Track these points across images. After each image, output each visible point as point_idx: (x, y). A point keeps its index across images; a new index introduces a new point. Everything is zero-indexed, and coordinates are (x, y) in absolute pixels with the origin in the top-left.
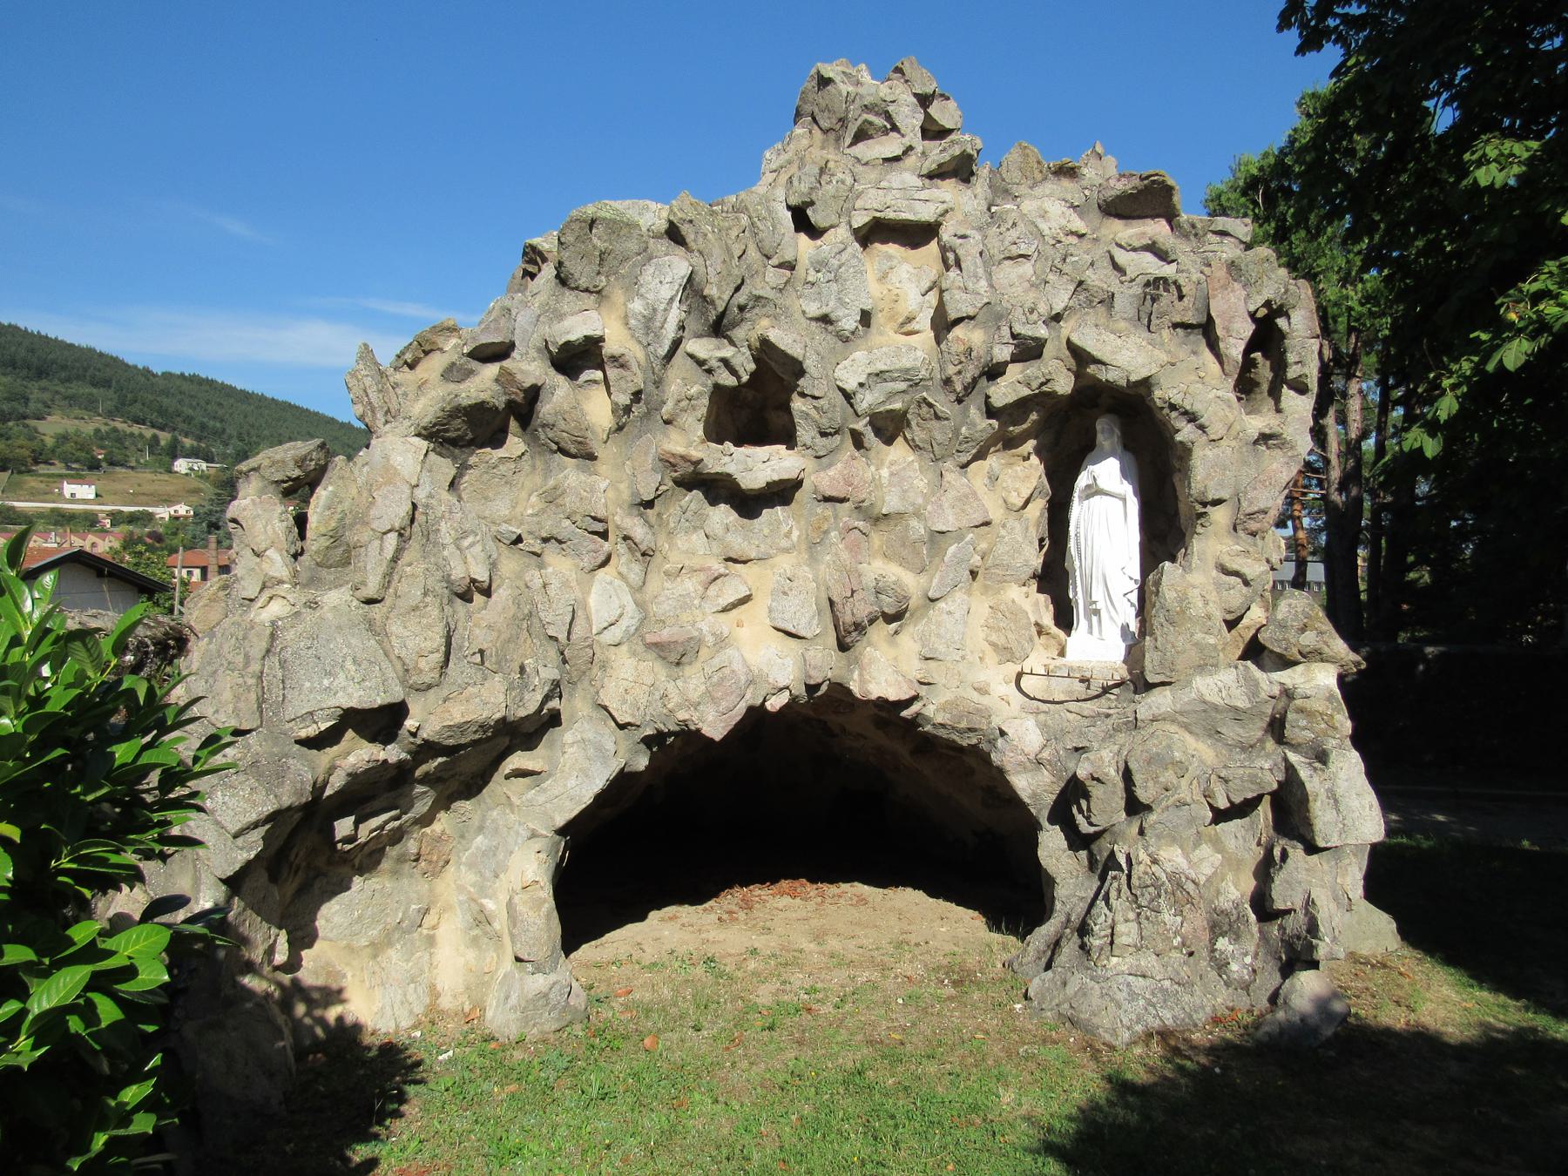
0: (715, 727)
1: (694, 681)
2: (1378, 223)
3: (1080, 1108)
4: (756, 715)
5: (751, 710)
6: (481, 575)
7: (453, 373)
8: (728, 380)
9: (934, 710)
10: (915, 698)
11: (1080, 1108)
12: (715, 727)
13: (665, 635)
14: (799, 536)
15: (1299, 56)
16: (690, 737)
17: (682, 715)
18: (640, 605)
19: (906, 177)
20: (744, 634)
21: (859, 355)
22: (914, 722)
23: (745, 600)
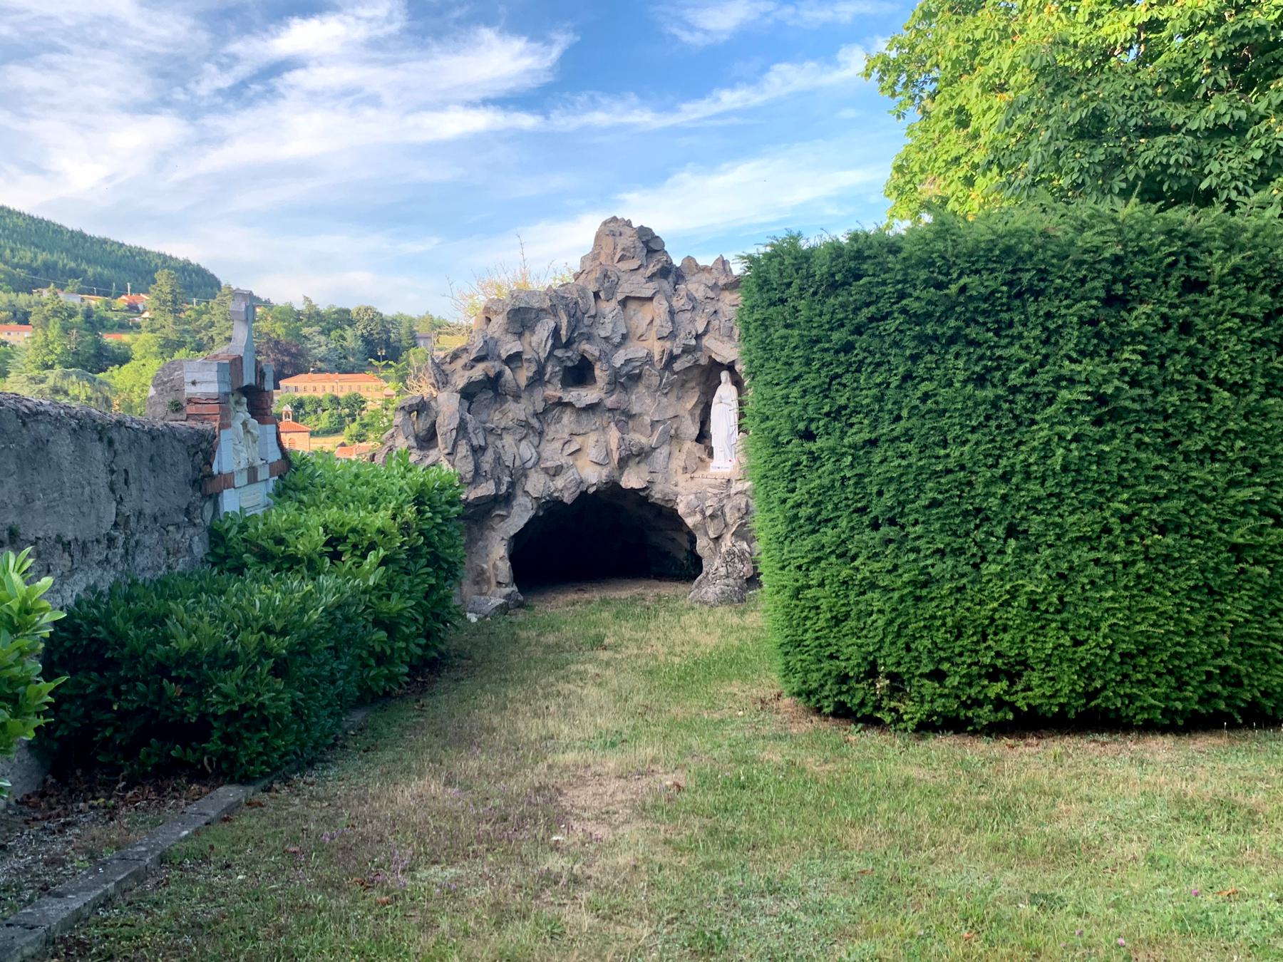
0: (568, 498)
1: (559, 482)
2: (110, 710)
3: (493, 529)
4: (584, 494)
5: (582, 493)
6: (483, 443)
7: (470, 366)
8: (569, 364)
9: (657, 495)
10: (646, 488)
11: (493, 529)
12: (568, 498)
13: (549, 464)
14: (1261, 29)
15: (795, 233)
16: (558, 502)
17: (556, 494)
18: (538, 453)
19: (640, 278)
20: (579, 463)
21: (622, 352)
22: (647, 497)
23: (579, 450)
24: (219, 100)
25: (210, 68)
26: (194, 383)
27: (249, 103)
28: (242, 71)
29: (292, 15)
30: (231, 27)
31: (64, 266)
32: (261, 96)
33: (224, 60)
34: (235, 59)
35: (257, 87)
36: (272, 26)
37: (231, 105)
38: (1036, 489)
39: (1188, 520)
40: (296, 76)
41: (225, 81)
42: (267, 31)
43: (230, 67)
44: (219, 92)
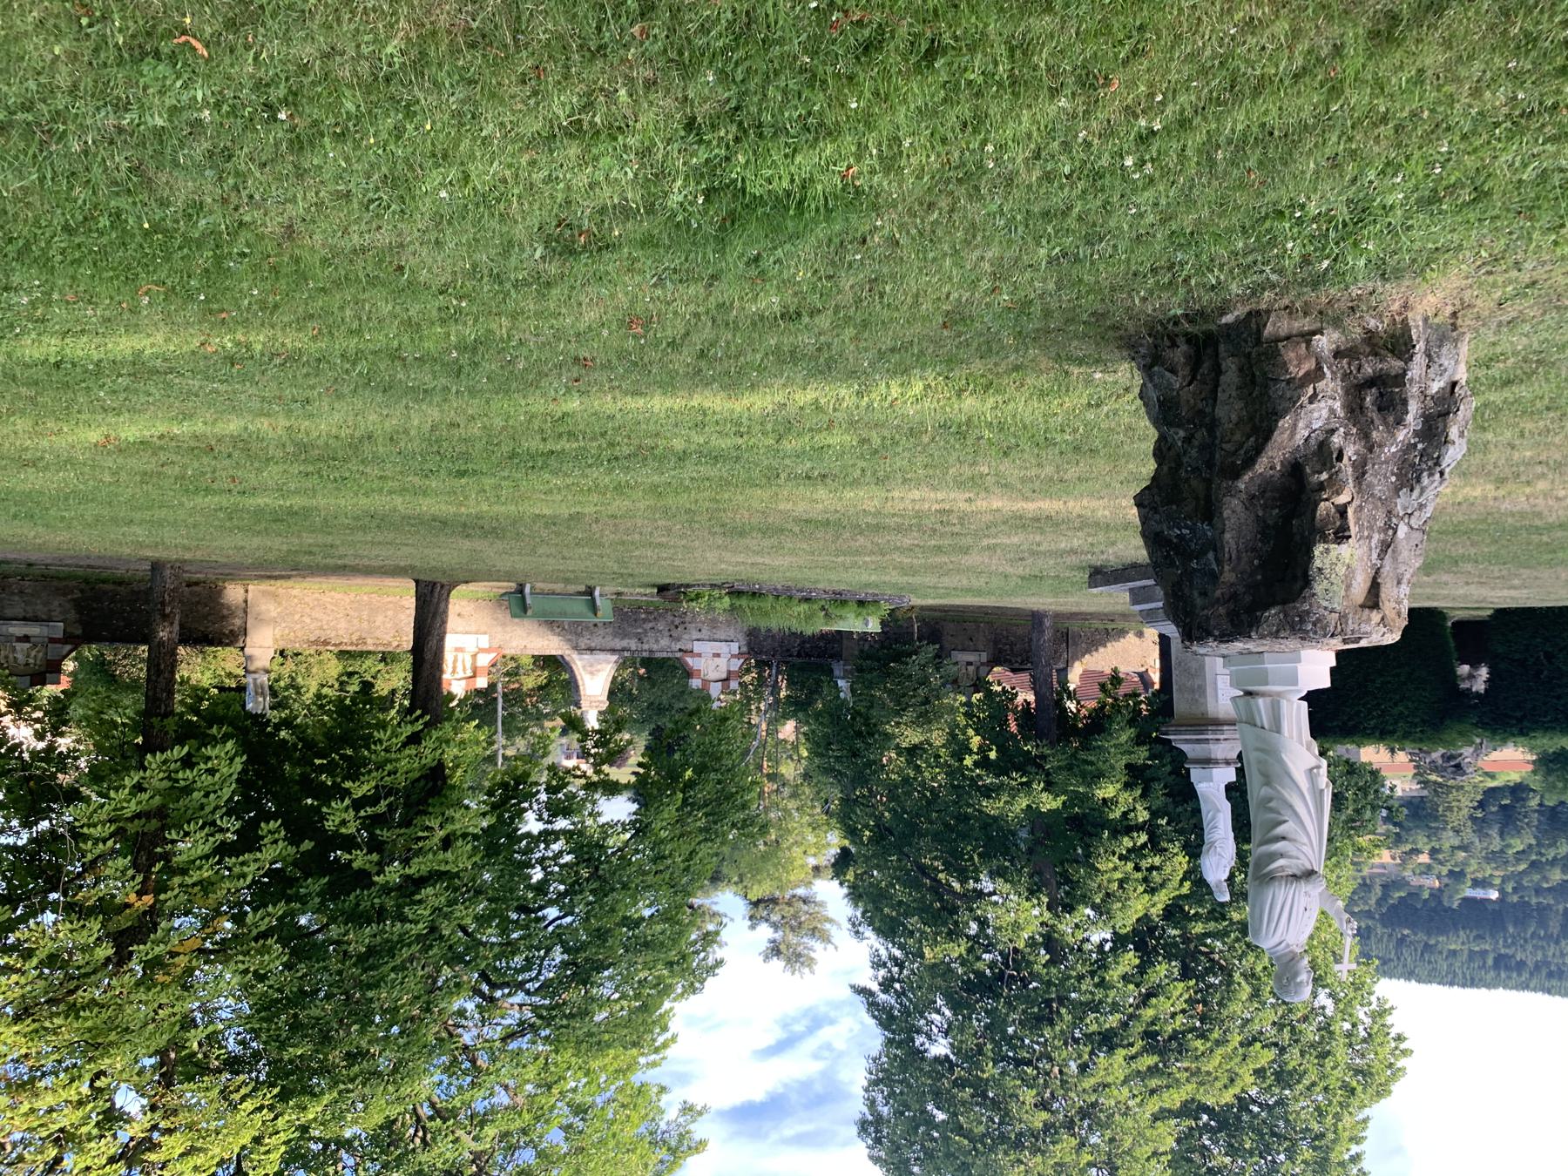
24: (833, 1014)
25: (840, 1045)
26: (718, 655)
27: (806, 1013)
28: (811, 1044)
29: (763, 1104)
30: (818, 1088)
31: (640, 765)
32: (796, 1020)
33: (826, 1054)
34: (816, 1056)
35: (799, 1028)
36: (781, 1090)
37: (823, 1009)
38: (637, 537)
39: (660, 523)
40: (770, 1040)
41: (825, 1034)
42: (785, 1085)
43: (821, 1048)
44: (832, 1022)
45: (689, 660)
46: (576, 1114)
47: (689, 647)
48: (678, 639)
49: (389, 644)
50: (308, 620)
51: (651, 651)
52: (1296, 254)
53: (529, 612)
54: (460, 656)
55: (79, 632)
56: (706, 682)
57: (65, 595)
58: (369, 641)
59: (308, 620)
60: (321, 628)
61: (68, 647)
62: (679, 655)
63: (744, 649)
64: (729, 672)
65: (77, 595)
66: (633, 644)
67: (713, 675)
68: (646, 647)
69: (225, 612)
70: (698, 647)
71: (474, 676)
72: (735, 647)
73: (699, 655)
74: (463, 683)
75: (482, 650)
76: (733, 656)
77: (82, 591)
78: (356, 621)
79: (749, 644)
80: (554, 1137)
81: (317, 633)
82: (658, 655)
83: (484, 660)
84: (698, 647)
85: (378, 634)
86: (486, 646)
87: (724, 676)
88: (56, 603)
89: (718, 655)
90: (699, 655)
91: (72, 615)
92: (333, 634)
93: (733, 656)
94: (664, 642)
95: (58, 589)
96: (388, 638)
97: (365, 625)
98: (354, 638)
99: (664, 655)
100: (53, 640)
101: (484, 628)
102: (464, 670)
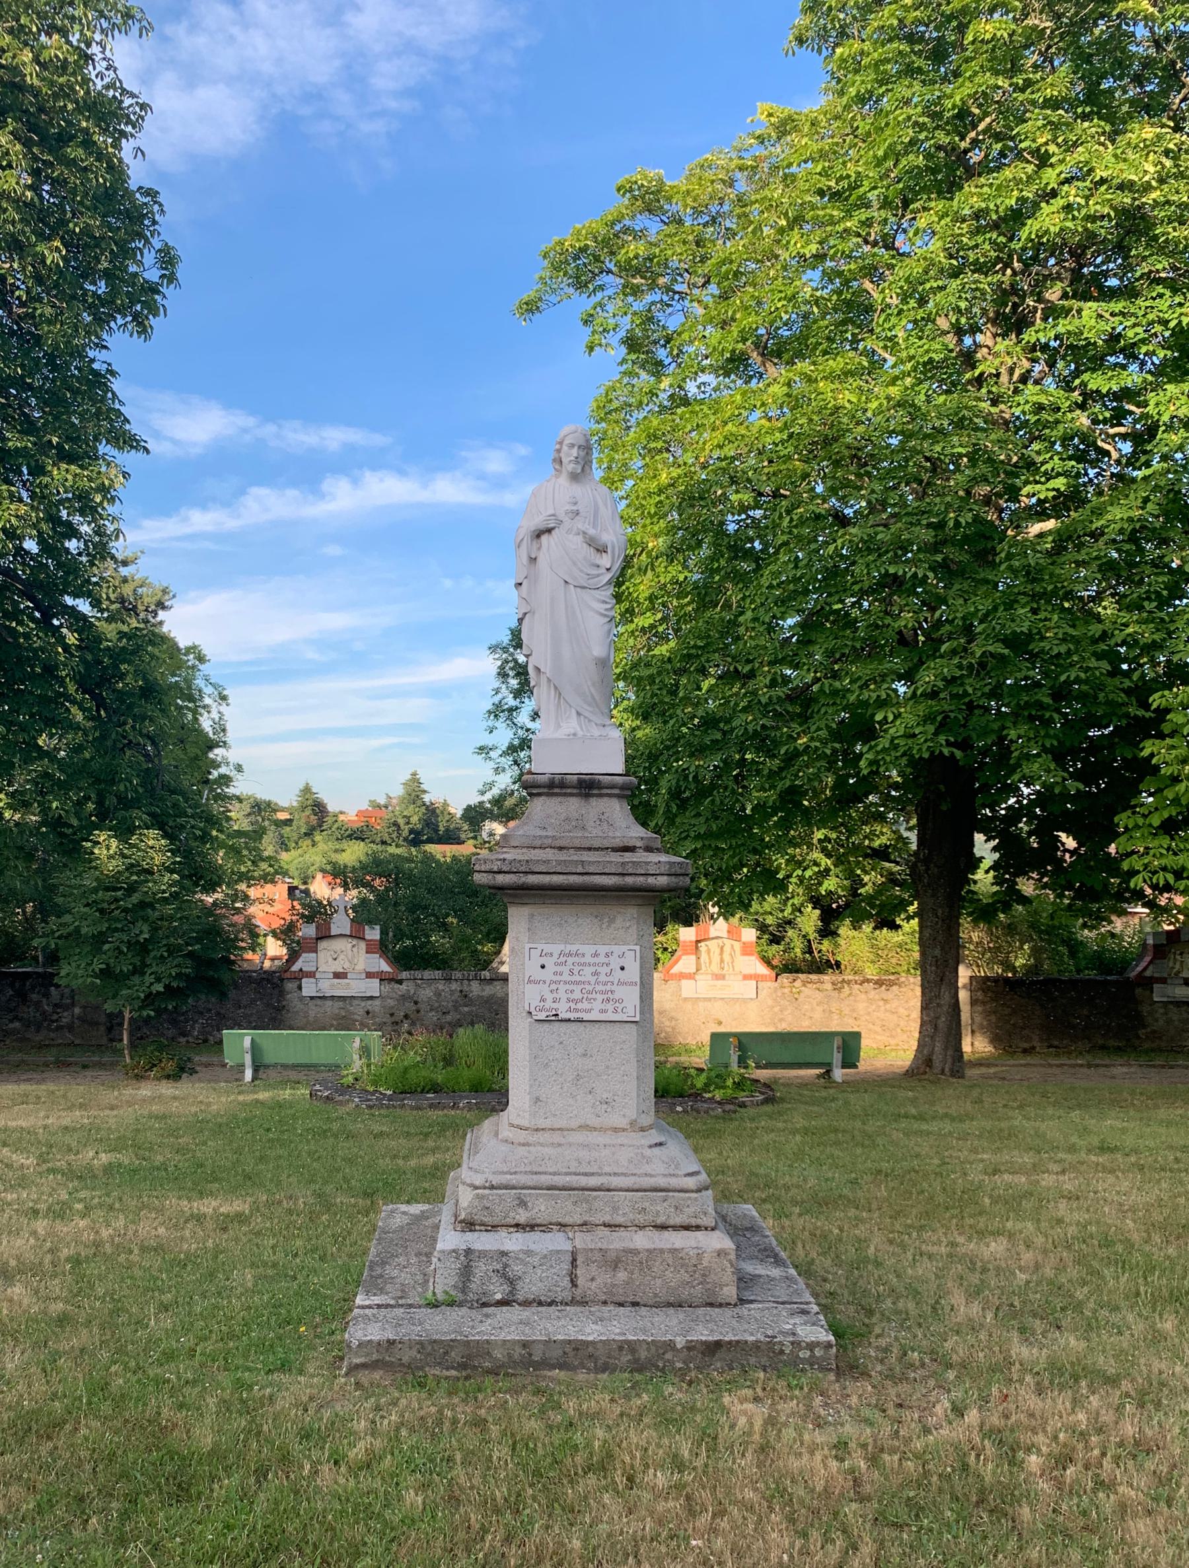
26: (337, 975)
45: (385, 967)
46: (950, 188)
47: (387, 988)
48: (404, 998)
49: (804, 984)
50: (901, 1010)
51: (448, 979)
52: (1035, 1240)
53: (837, 1042)
54: (715, 968)
55: (1138, 991)
56: (357, 935)
57: (1154, 1032)
58: (829, 986)
59: (901, 1010)
60: (885, 1001)
61: (1148, 973)
62: (404, 975)
63: (290, 986)
64: (315, 950)
65: (1141, 1032)
66: (475, 988)
67: (343, 945)
68: (455, 986)
69: (993, 1018)
70: (373, 987)
71: (698, 942)
72: (309, 988)
73: (369, 975)
74: (713, 933)
75: (690, 976)
76: (312, 975)
77: (1138, 1037)
78: (846, 1011)
79: (282, 993)
80: (984, 88)
81: (889, 996)
82: (438, 974)
83: (686, 963)
84: (373, 987)
85: (819, 995)
86: (684, 982)
87: (323, 945)
88: (1161, 1022)
89: (337, 975)
90: (369, 975)
91: (1145, 1009)
92: (872, 994)
93: (312, 975)
94: (426, 993)
95: (1160, 1038)
96: (806, 991)
97: (834, 1006)
98: (846, 990)
99: (427, 974)
100: (1163, 981)
101: (689, 1006)
102: (709, 951)
